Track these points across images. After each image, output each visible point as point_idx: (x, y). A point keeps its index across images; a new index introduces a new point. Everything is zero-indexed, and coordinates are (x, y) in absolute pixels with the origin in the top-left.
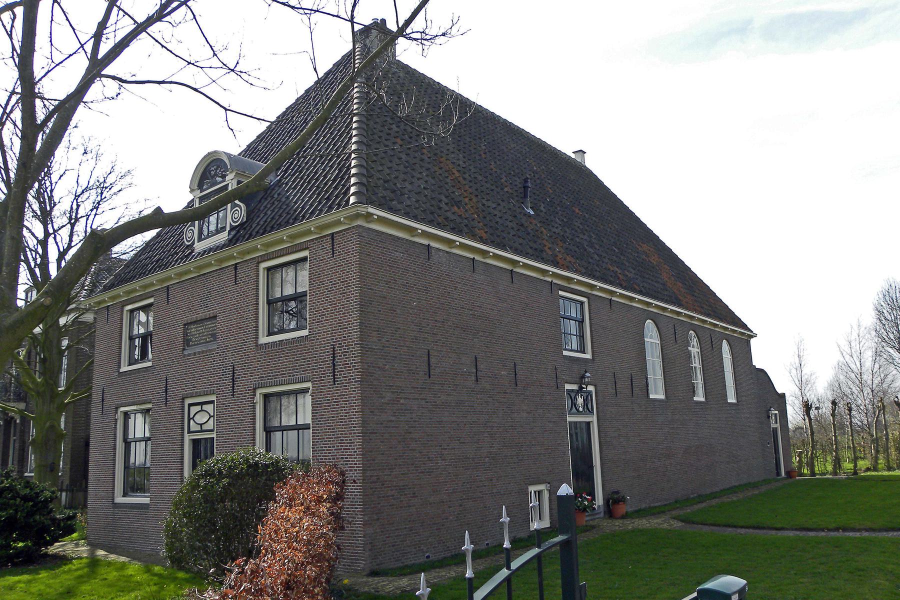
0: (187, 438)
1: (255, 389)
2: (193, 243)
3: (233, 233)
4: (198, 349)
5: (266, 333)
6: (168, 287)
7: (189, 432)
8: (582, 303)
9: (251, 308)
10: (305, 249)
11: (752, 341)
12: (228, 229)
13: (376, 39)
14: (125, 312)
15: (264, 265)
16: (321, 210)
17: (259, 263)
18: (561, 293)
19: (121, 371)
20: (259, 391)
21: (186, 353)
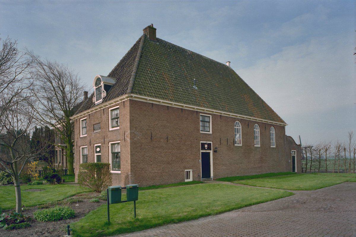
0: (96, 154)
1: (109, 142)
2: (95, 102)
3: (103, 99)
4: (97, 131)
5: (82, 134)
6: (89, 114)
7: (96, 153)
8: (209, 117)
9: (107, 121)
10: (118, 105)
11: (286, 127)
12: (102, 98)
13: (151, 30)
14: (109, 111)
15: (110, 109)
16: (123, 94)
17: (109, 109)
18: (201, 114)
19: (81, 137)
20: (81, 147)
21: (94, 132)
